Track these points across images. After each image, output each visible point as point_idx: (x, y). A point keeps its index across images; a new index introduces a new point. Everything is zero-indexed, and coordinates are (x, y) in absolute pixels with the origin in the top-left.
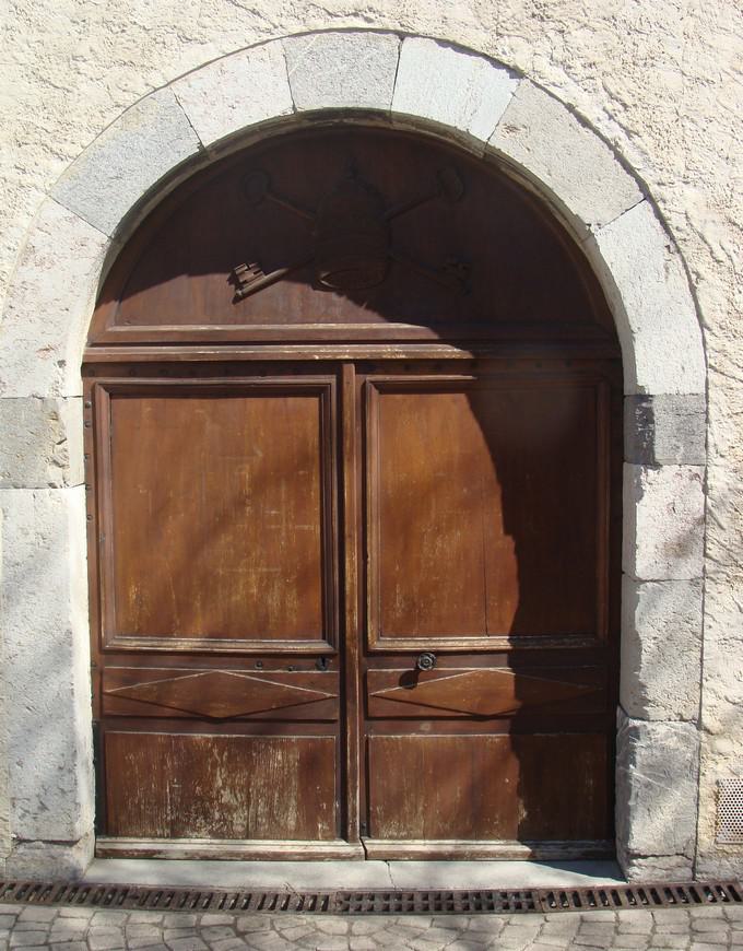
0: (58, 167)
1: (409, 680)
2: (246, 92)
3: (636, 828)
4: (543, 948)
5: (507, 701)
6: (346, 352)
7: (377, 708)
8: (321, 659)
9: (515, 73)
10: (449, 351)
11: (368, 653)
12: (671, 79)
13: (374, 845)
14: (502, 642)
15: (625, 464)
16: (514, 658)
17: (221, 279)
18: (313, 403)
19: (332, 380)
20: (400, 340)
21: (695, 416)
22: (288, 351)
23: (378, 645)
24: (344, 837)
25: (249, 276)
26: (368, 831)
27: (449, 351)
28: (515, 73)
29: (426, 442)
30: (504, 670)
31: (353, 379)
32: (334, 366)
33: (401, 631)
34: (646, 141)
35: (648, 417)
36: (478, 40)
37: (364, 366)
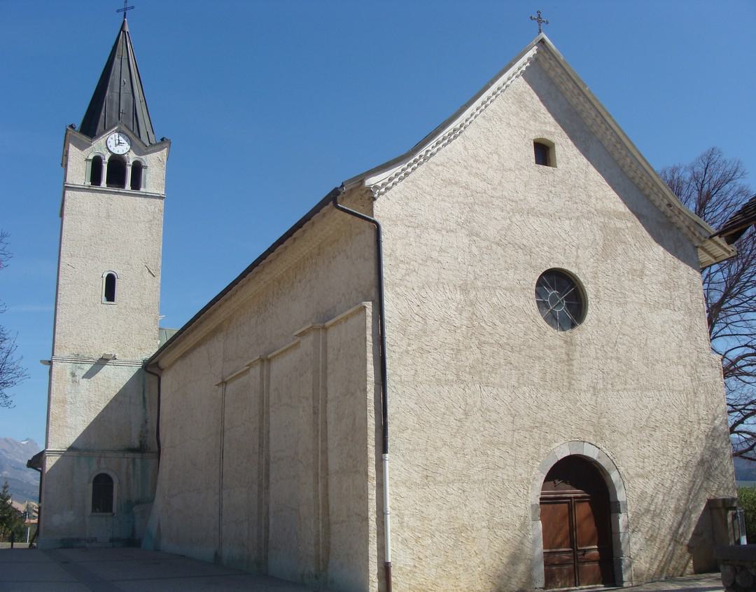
0: (538, 463)
1: (583, 555)
2: (563, 452)
3: (624, 577)
4: (646, 590)
5: (599, 558)
6: (572, 495)
7: (579, 560)
8: (570, 551)
9: (599, 448)
10: (586, 495)
11: (578, 550)
12: (619, 450)
13: (580, 587)
14: (596, 547)
15: (612, 515)
16: (598, 549)
17: (552, 482)
18: (566, 505)
19: (569, 500)
20: (579, 493)
21: (625, 504)
22: (564, 495)
23: (579, 548)
24: (576, 586)
25: (557, 482)
26: (579, 585)
27: (586, 495)
28: (599, 448)
29: (583, 510)
30: (597, 552)
31: (573, 500)
32: (570, 498)
33: (582, 546)
34: (616, 460)
35: (619, 505)
36: (594, 443)
37: (575, 498)
